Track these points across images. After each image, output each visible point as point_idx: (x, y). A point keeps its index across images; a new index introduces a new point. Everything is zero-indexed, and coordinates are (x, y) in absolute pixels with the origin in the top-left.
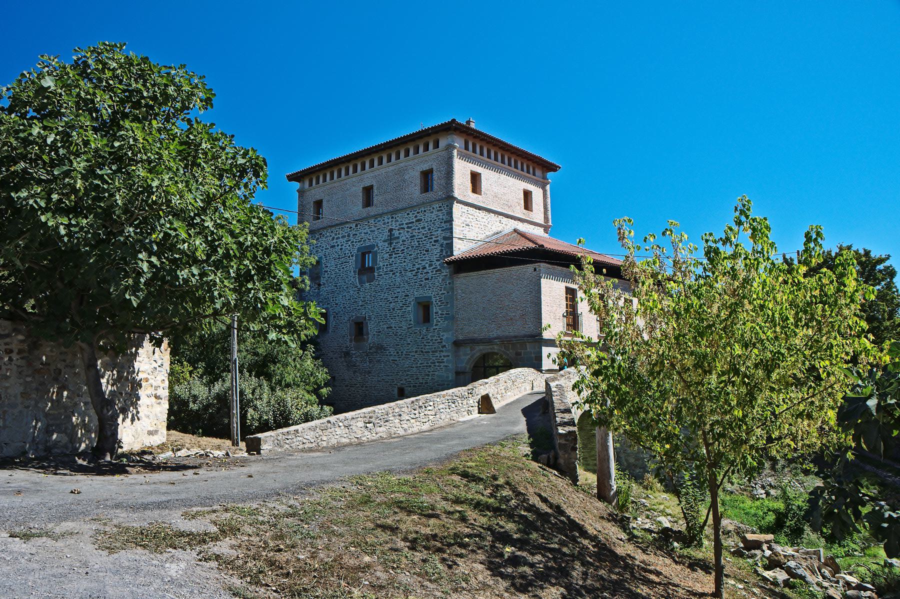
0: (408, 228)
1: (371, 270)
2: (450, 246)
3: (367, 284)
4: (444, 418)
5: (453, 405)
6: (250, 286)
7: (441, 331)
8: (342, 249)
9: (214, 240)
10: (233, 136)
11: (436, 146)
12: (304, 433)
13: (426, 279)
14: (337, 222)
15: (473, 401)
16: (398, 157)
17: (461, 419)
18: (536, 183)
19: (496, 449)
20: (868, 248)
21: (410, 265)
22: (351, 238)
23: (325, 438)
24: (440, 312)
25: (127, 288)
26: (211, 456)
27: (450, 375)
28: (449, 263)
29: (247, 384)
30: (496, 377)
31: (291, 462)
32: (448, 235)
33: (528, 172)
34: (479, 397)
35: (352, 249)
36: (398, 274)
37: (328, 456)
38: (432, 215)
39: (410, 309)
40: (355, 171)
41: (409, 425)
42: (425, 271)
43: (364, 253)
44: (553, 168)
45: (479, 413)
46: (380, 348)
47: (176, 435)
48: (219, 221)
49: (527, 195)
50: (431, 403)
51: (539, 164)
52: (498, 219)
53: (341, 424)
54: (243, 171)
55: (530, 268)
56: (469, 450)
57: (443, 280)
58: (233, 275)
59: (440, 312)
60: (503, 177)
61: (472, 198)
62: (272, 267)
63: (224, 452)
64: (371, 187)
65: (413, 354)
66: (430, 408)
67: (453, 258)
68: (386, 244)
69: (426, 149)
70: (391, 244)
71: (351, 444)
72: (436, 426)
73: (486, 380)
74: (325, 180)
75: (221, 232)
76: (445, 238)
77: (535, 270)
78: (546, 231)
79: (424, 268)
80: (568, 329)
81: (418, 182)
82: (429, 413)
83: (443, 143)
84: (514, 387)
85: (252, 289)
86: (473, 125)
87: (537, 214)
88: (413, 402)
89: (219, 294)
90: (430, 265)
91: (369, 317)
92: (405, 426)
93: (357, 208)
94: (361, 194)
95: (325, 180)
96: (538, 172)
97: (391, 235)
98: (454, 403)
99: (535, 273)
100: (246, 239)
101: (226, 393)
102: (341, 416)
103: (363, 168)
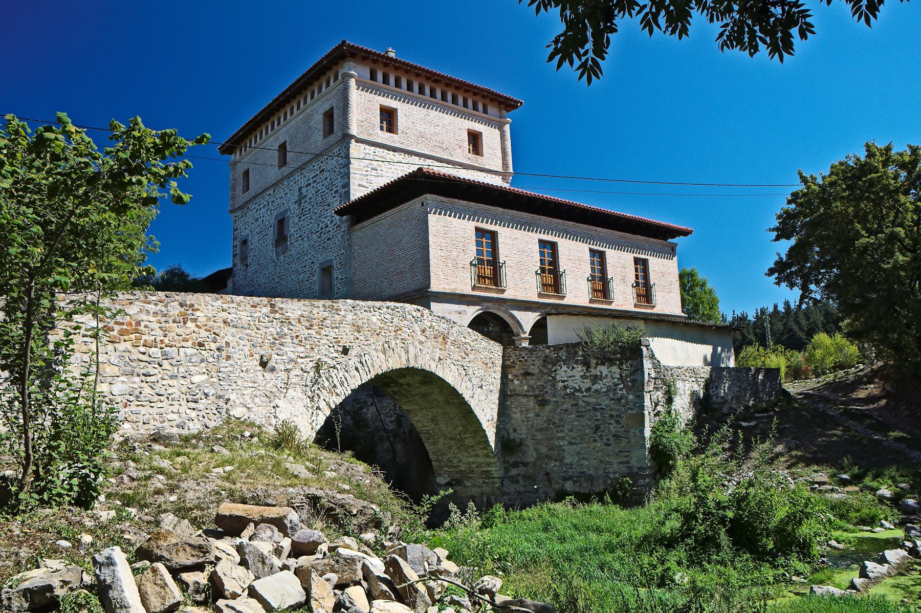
0: (314, 182)
13: (329, 239)
18: (489, 123)
20: (914, 144)
32: (346, 181)
35: (270, 219)
39: (315, 278)
42: (327, 229)
43: (281, 223)
49: (475, 139)
51: (492, 100)
55: (417, 201)
60: (434, 115)
77: (423, 204)
81: (321, 126)
90: (332, 222)
93: (274, 173)
96: (493, 110)
97: (301, 194)
99: (422, 209)
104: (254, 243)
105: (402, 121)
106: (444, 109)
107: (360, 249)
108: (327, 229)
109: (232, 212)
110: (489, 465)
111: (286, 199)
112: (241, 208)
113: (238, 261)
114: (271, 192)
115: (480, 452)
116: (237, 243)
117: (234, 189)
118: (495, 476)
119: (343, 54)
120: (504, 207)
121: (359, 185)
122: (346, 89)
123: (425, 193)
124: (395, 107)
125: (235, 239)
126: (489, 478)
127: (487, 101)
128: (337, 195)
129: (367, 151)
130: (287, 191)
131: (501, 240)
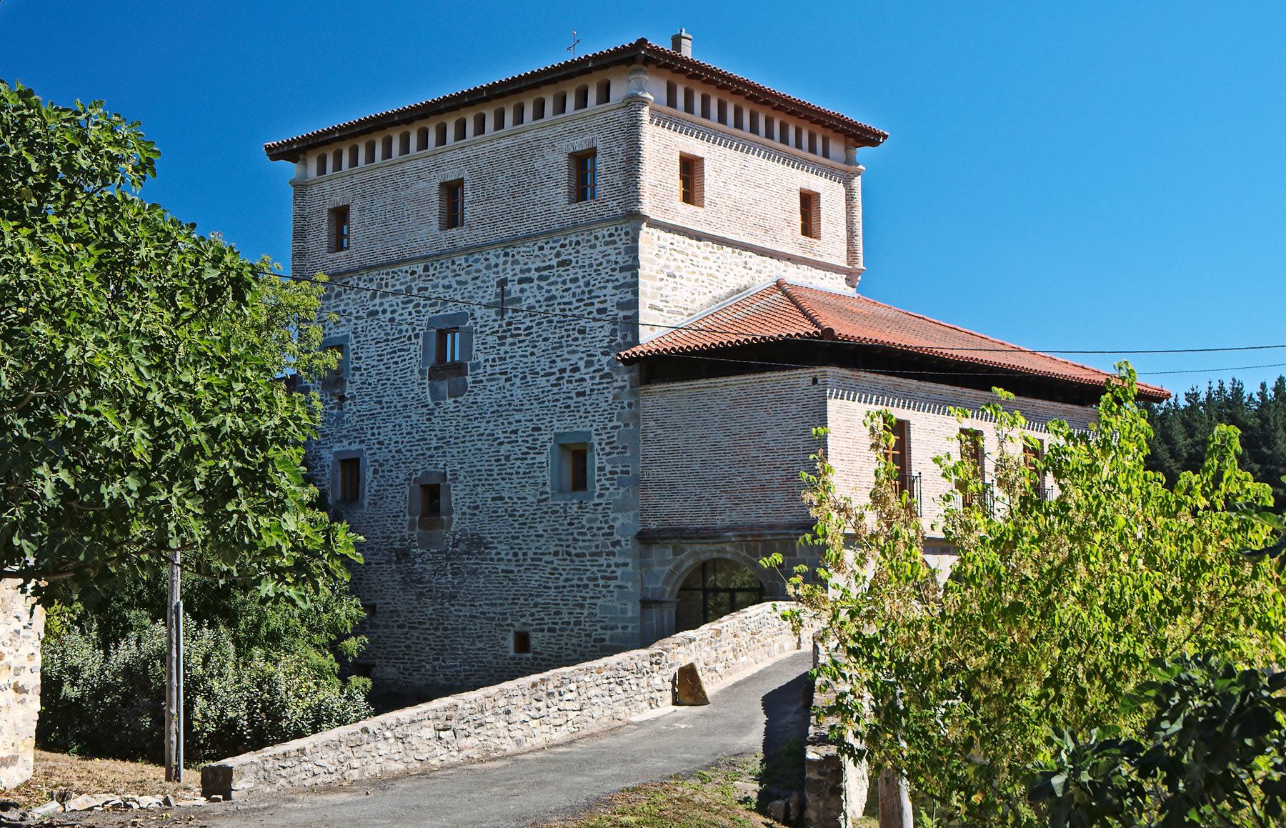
1: (459, 369)
2: (632, 324)
4: (600, 715)
5: (619, 689)
6: (230, 507)
7: (612, 511)
8: (389, 328)
9: (165, 426)
10: (193, 226)
11: (604, 97)
12: (319, 752)
13: (580, 394)
14: (384, 259)
15: (662, 680)
16: (519, 119)
17: (636, 718)
18: (830, 173)
19: (685, 789)
21: (545, 362)
23: (356, 763)
24: (608, 468)
25: (14, 526)
26: (135, 806)
27: (629, 606)
28: (628, 362)
29: (189, 644)
30: (715, 625)
31: (294, 816)
32: (629, 297)
33: (812, 149)
34: (675, 669)
36: (518, 381)
37: (364, 802)
38: (596, 252)
39: (542, 458)
40: (423, 144)
41: (527, 731)
42: (577, 376)
44: (868, 138)
45: (675, 703)
46: (477, 543)
47: (67, 764)
48: (173, 391)
49: (809, 201)
50: (573, 686)
51: (836, 130)
52: (740, 260)
53: (388, 734)
54: (214, 292)
55: (803, 376)
56: (634, 790)
57: (615, 397)
58: (199, 487)
59: (608, 468)
61: (684, 215)
62: (270, 470)
63: (160, 798)
64: (460, 182)
65: (549, 558)
66: (569, 696)
67: (637, 349)
69: (582, 102)
70: (502, 313)
71: (406, 775)
72: (583, 732)
73: (690, 633)
74: (354, 162)
75: (176, 410)
76: (620, 306)
77: (815, 381)
78: (850, 281)
79: (576, 370)
81: (563, 176)
82: (568, 706)
83: (618, 92)
84: (748, 648)
85: (234, 512)
86: (687, 51)
87: (832, 244)
88: (534, 685)
89: (177, 527)
90: (589, 364)
91: (454, 473)
92: (518, 734)
93: (427, 229)
94: (436, 198)
95: (354, 162)
96: (836, 148)
97: (503, 293)
98: (620, 684)
99: (814, 389)
100: (224, 421)
101: (146, 663)
102: (390, 717)
103: (442, 140)
105: (711, 181)
106: (771, 154)
107: (661, 426)
108: (577, 376)
114: (419, 268)
119: (636, 57)
127: (829, 133)
129: (662, 243)
131: (915, 435)
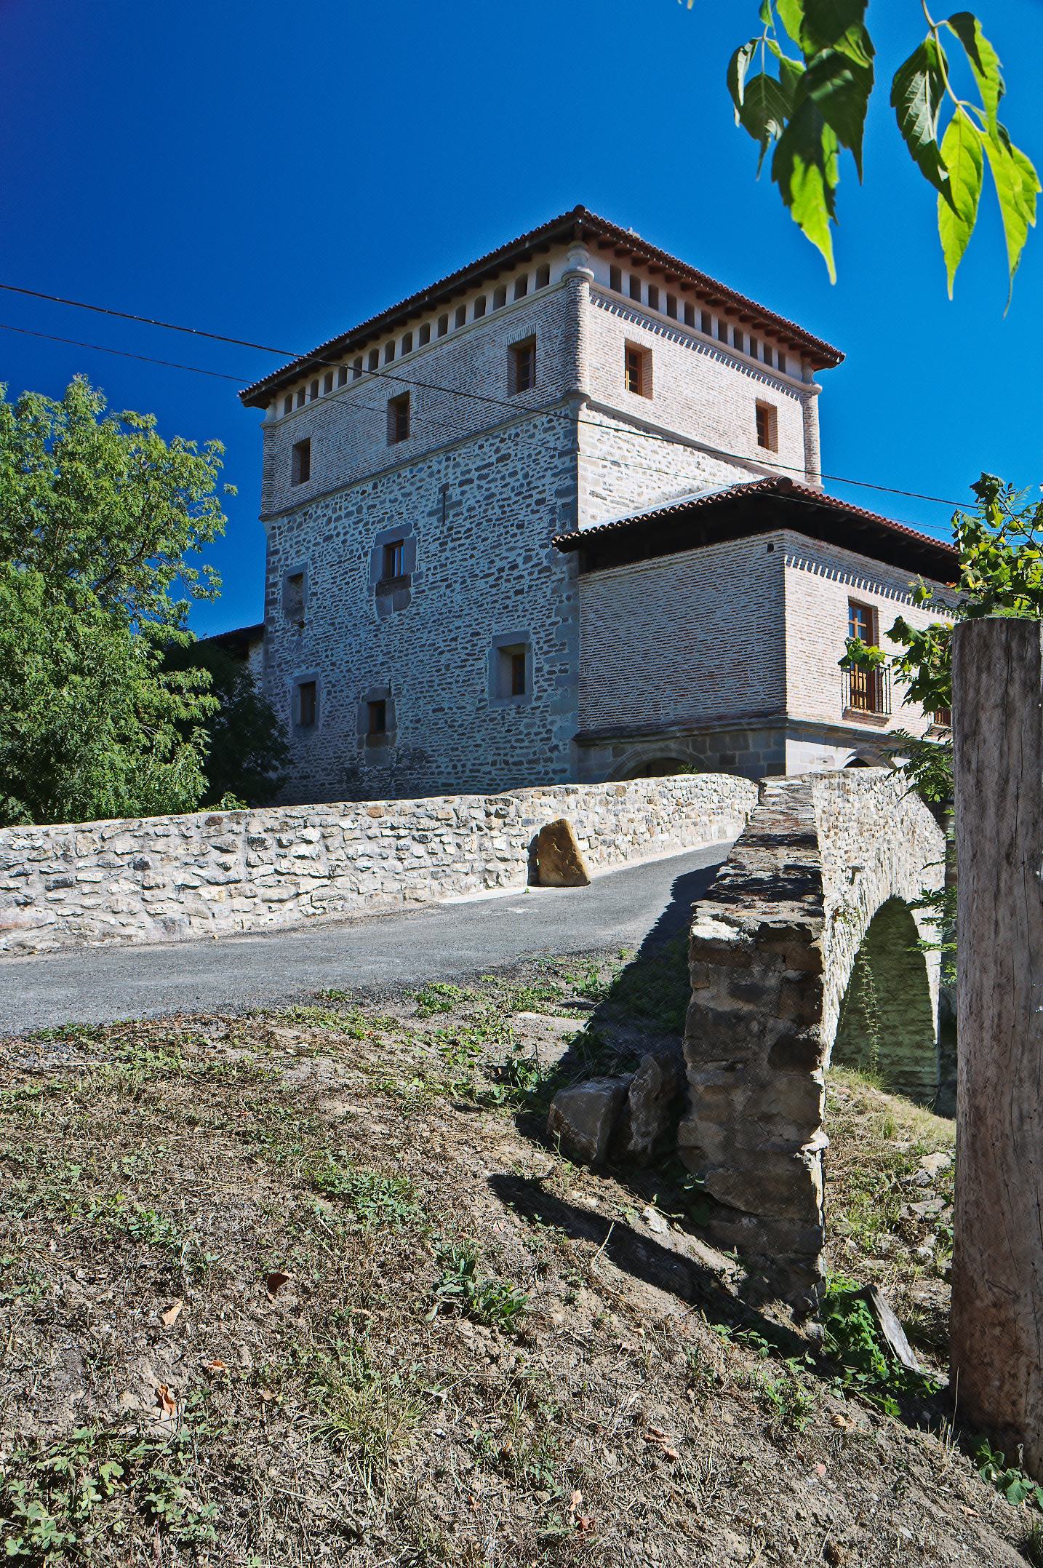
0: (481, 477)
1: (404, 581)
2: (571, 511)
3: (394, 615)
5: (419, 849)
11: (544, 279)
14: (338, 483)
15: (510, 843)
16: (461, 320)
18: (787, 388)
21: (484, 563)
22: (364, 516)
24: (546, 668)
32: (568, 482)
34: (535, 830)
36: (457, 586)
39: (481, 664)
42: (516, 573)
43: (392, 548)
49: (765, 415)
50: (313, 834)
51: (793, 347)
55: (758, 542)
57: (554, 591)
59: (546, 668)
60: (708, 365)
66: (304, 849)
68: (434, 520)
77: (770, 548)
79: (514, 567)
80: (855, 704)
81: (503, 370)
82: (300, 867)
83: (556, 275)
90: (527, 559)
92: (173, 910)
96: (792, 365)
97: (445, 498)
98: (423, 840)
99: (769, 557)
104: (321, 580)
105: (659, 374)
106: (724, 357)
107: (601, 618)
109: (264, 518)
110: (917, 1061)
111: (408, 502)
112: (289, 512)
113: (278, 613)
114: (368, 487)
115: (906, 1039)
116: (277, 578)
117: (270, 473)
118: (926, 1081)
120: (889, 562)
121: (593, 494)
122: (574, 303)
123: (782, 527)
124: (648, 346)
125: (270, 571)
126: (912, 1085)
128: (542, 508)
130: (409, 488)
